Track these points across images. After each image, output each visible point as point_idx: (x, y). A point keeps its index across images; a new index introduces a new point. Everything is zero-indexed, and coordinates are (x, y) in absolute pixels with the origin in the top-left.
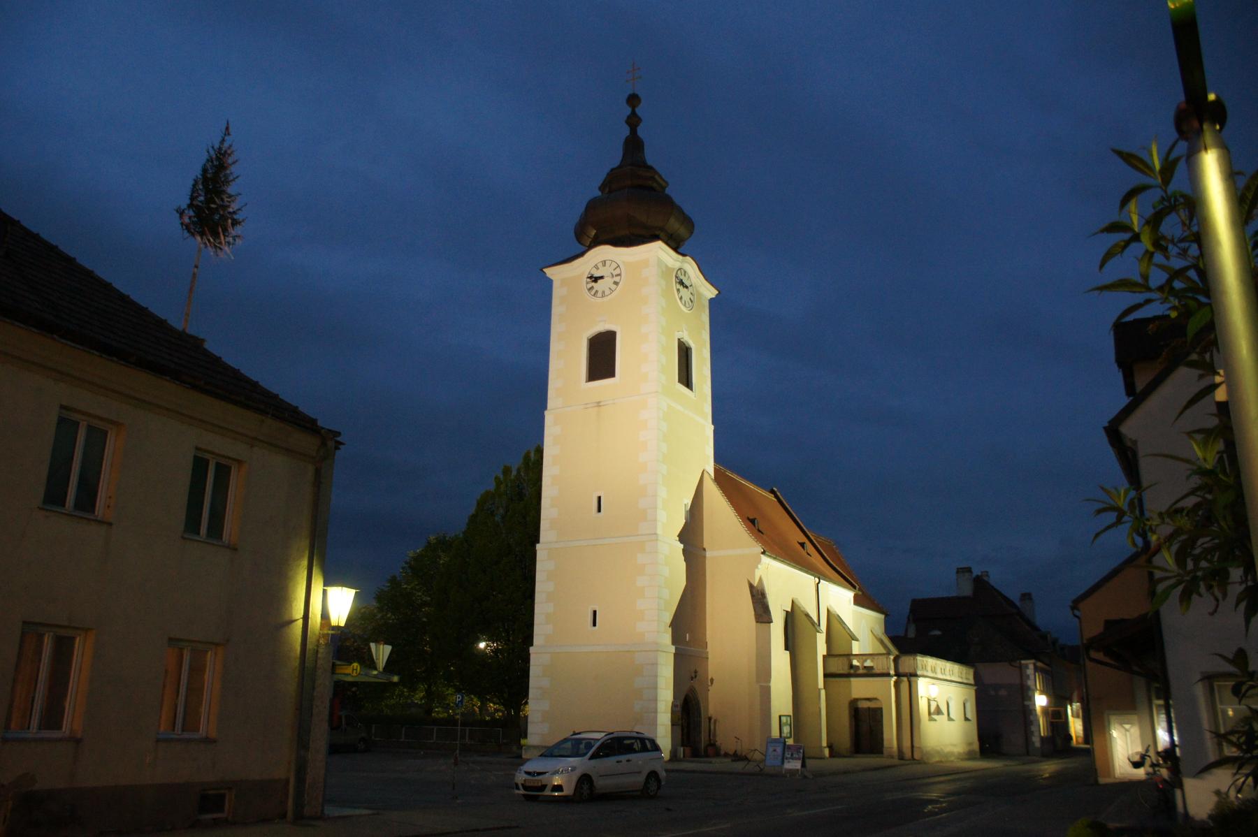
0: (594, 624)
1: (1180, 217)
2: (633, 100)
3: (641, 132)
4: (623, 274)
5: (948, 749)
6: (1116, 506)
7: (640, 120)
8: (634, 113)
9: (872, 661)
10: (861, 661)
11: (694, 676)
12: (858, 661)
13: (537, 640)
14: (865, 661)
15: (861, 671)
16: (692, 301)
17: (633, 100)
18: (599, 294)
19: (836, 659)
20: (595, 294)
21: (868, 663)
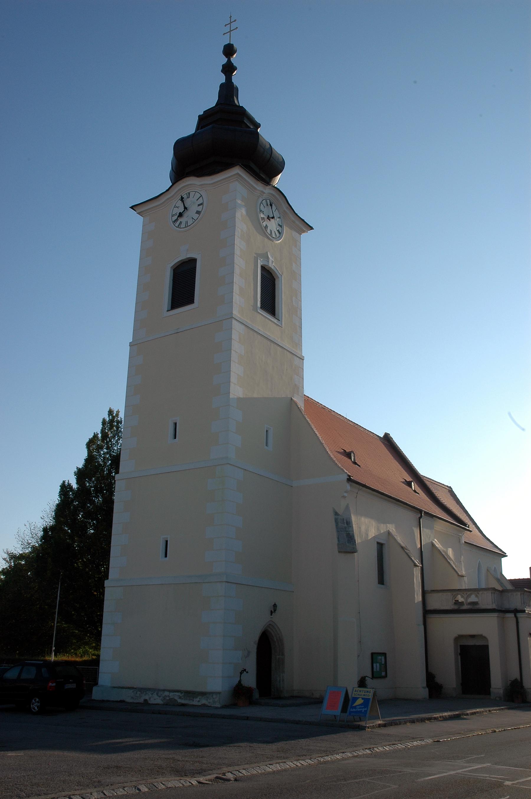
0: (166, 556)
1: (495, 604)
2: (229, 50)
3: (236, 78)
4: (205, 204)
5: (240, 168)
6: (310, 738)
7: (234, 69)
8: (229, 61)
9: (477, 596)
10: (465, 596)
11: (273, 611)
12: (462, 597)
13: (113, 573)
14: (469, 596)
15: (465, 607)
16: (280, 233)
17: (229, 50)
18: (183, 225)
19: (440, 594)
20: (178, 226)
21: (473, 598)
